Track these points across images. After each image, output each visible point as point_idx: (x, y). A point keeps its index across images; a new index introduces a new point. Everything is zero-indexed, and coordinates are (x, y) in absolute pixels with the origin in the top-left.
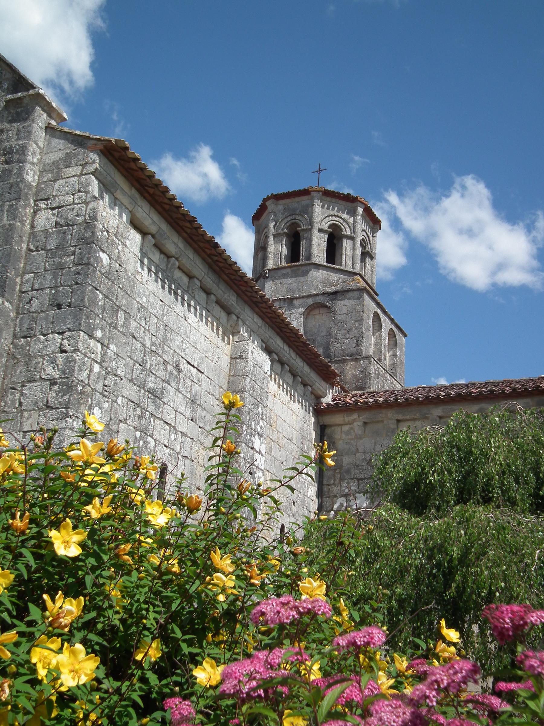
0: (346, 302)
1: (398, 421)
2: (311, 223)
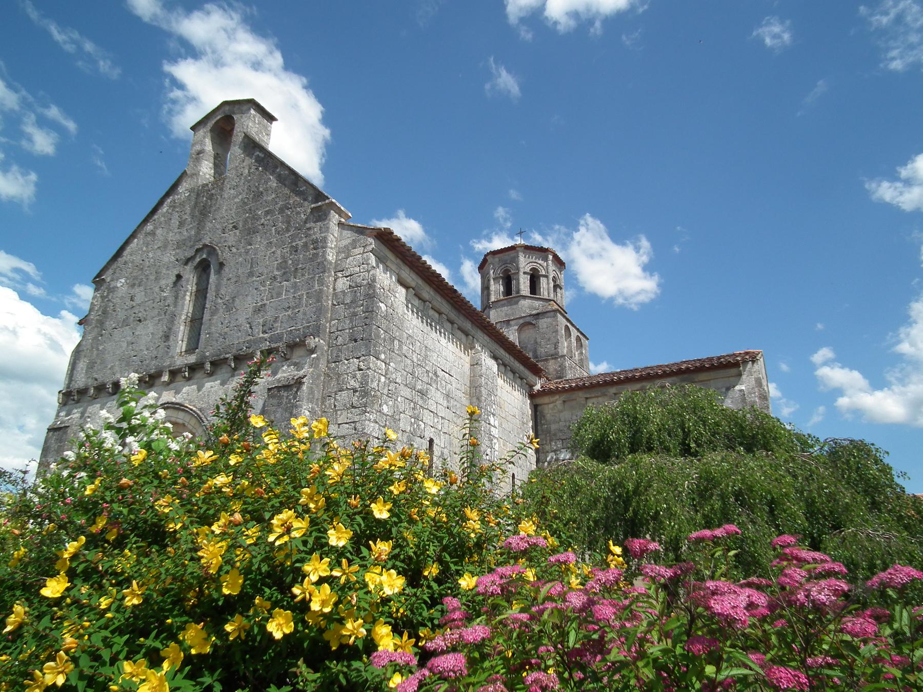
0: (545, 320)
1: (587, 398)
2: (518, 269)
